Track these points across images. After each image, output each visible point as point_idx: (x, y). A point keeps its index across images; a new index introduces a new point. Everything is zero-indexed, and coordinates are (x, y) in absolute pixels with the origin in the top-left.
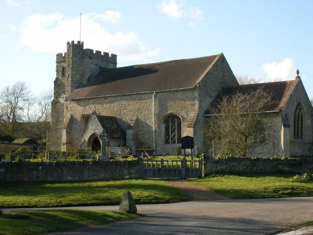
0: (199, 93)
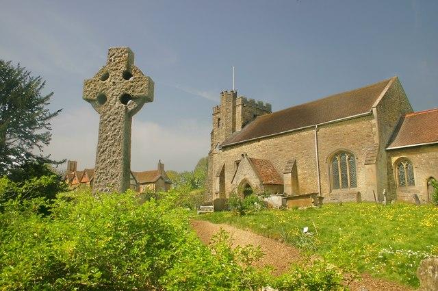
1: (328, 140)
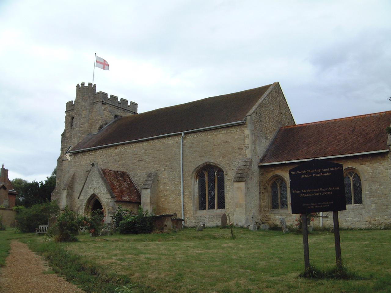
0: (252, 131)
1: (196, 151)
